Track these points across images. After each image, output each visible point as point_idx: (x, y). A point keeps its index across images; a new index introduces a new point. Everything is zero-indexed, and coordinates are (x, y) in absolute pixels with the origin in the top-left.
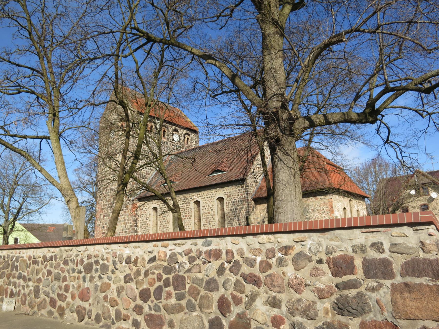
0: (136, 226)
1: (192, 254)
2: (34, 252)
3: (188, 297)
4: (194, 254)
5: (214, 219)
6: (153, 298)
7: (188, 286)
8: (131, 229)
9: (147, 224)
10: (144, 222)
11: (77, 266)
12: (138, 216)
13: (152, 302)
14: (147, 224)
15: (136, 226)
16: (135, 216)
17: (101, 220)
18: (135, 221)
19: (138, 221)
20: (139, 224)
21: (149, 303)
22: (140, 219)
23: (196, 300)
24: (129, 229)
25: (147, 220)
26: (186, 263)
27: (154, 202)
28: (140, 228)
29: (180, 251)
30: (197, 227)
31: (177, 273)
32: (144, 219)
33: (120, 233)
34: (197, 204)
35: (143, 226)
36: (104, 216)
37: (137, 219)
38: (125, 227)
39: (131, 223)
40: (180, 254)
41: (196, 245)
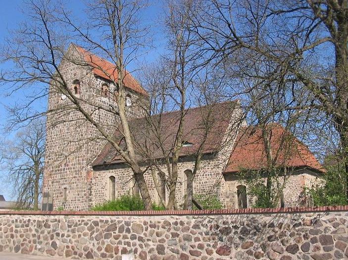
0: (90, 195)
1: (336, 221)
2: (150, 218)
3: (336, 249)
4: (338, 221)
5: (180, 192)
6: (300, 250)
7: (335, 242)
8: (85, 197)
9: (103, 193)
10: (99, 191)
11: (211, 230)
12: (93, 184)
13: (300, 253)
14: (103, 193)
15: (90, 195)
16: (90, 184)
17: (50, 186)
18: (90, 189)
19: (93, 189)
20: (93, 193)
21: (297, 254)
22: (94, 187)
23: (343, 251)
24: (82, 197)
25: (103, 190)
26: (331, 227)
27: (111, 171)
28: (94, 197)
29: (325, 219)
30: (111, 198)
31: (323, 233)
32: (99, 188)
33: (72, 200)
34: (111, 180)
35: (98, 195)
36: (52, 183)
37: (91, 187)
38: (78, 195)
39: (84, 191)
40: (325, 221)
41: (340, 215)
